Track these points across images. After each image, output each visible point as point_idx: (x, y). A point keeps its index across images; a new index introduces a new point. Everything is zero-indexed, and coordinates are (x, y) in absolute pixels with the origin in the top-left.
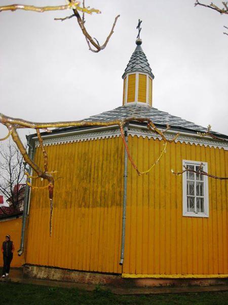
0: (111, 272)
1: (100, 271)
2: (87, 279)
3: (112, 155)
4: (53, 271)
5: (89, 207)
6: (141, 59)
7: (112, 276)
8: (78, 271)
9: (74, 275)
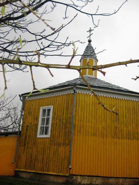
0: (135, 177)
1: (128, 177)
2: (120, 182)
3: (131, 111)
4: (95, 179)
5: (119, 138)
6: (91, 50)
7: (136, 180)
8: (114, 178)
9: (111, 181)
